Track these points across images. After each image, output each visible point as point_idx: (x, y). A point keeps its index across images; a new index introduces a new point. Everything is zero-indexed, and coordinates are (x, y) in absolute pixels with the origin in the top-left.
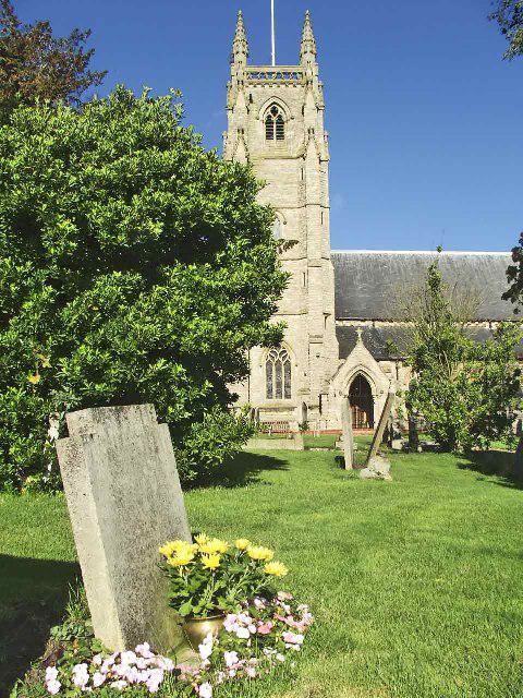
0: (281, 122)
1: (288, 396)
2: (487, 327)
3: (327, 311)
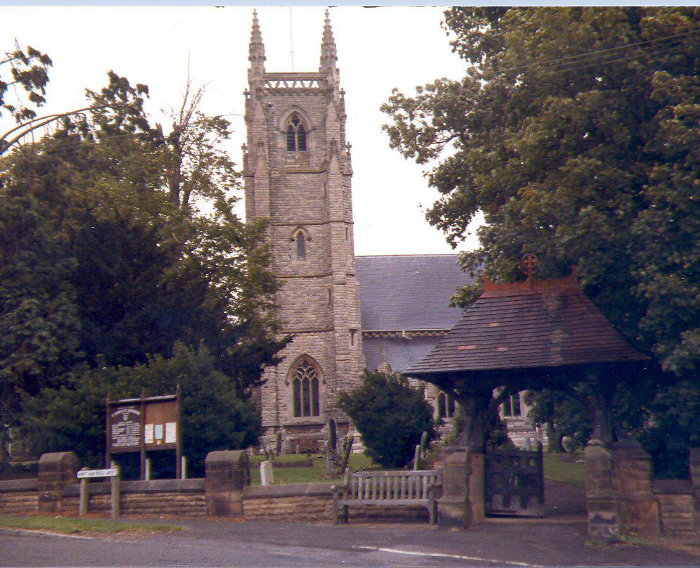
1: (317, 413)
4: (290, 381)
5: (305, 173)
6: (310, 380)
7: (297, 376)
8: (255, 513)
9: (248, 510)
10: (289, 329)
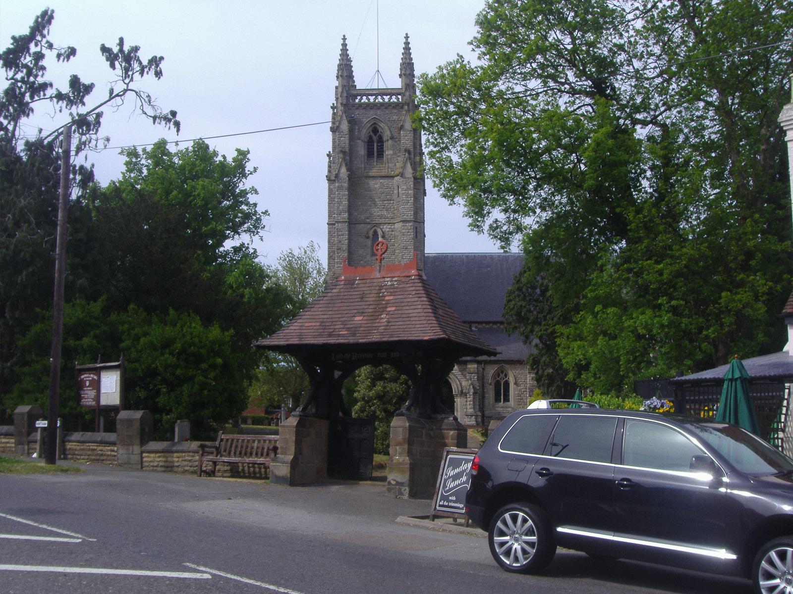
0: (381, 141)
5: (382, 177)
8: (152, 464)
9: (146, 461)
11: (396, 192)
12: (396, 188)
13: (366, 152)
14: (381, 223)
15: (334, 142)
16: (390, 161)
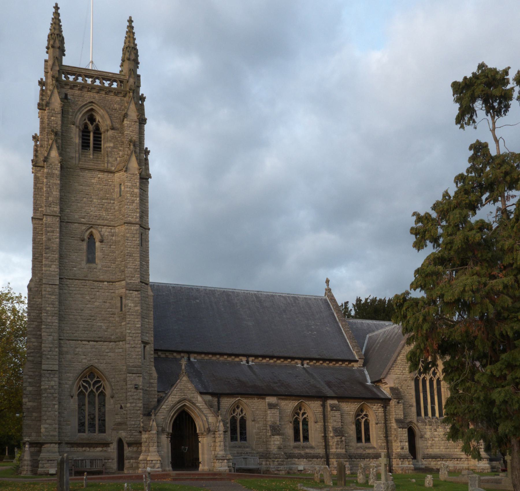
0: (97, 132)
1: (102, 430)
2: (244, 362)
3: (146, 339)
4: (75, 392)
6: (97, 394)
7: (82, 388)
10: (76, 337)
11: (117, 190)
12: (118, 186)
13: (81, 142)
14: (98, 225)
15: (42, 122)
16: (110, 155)
